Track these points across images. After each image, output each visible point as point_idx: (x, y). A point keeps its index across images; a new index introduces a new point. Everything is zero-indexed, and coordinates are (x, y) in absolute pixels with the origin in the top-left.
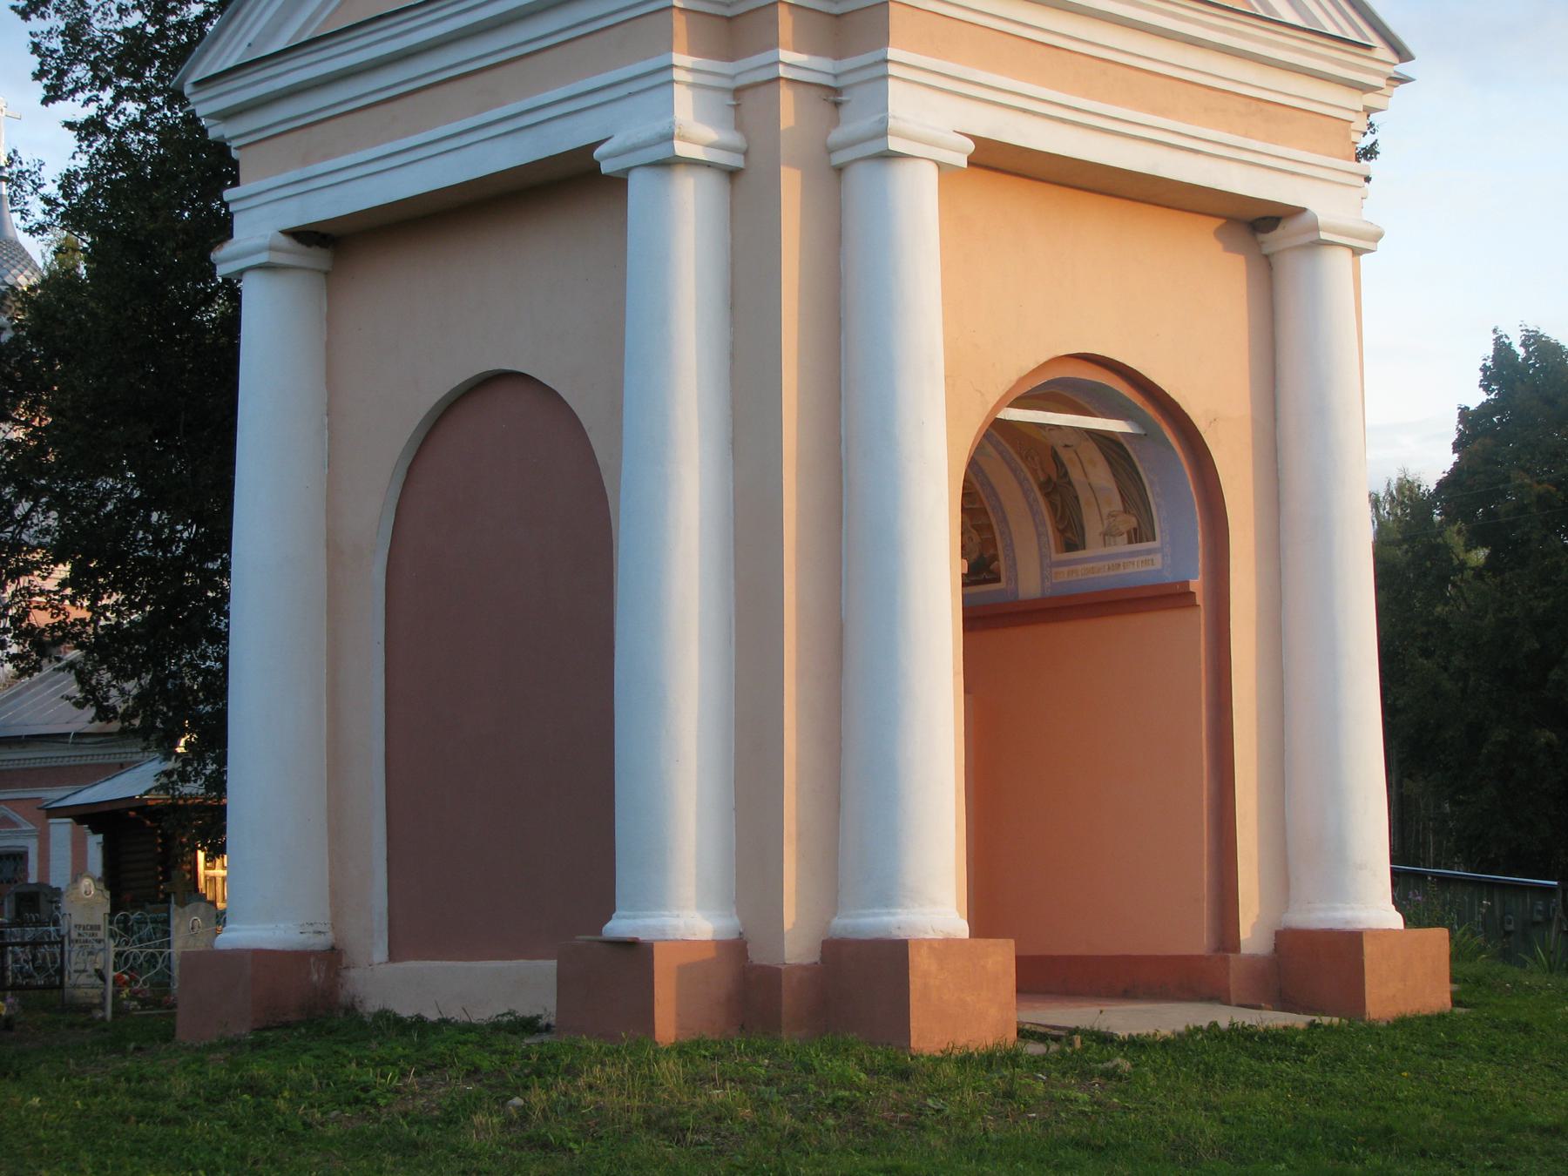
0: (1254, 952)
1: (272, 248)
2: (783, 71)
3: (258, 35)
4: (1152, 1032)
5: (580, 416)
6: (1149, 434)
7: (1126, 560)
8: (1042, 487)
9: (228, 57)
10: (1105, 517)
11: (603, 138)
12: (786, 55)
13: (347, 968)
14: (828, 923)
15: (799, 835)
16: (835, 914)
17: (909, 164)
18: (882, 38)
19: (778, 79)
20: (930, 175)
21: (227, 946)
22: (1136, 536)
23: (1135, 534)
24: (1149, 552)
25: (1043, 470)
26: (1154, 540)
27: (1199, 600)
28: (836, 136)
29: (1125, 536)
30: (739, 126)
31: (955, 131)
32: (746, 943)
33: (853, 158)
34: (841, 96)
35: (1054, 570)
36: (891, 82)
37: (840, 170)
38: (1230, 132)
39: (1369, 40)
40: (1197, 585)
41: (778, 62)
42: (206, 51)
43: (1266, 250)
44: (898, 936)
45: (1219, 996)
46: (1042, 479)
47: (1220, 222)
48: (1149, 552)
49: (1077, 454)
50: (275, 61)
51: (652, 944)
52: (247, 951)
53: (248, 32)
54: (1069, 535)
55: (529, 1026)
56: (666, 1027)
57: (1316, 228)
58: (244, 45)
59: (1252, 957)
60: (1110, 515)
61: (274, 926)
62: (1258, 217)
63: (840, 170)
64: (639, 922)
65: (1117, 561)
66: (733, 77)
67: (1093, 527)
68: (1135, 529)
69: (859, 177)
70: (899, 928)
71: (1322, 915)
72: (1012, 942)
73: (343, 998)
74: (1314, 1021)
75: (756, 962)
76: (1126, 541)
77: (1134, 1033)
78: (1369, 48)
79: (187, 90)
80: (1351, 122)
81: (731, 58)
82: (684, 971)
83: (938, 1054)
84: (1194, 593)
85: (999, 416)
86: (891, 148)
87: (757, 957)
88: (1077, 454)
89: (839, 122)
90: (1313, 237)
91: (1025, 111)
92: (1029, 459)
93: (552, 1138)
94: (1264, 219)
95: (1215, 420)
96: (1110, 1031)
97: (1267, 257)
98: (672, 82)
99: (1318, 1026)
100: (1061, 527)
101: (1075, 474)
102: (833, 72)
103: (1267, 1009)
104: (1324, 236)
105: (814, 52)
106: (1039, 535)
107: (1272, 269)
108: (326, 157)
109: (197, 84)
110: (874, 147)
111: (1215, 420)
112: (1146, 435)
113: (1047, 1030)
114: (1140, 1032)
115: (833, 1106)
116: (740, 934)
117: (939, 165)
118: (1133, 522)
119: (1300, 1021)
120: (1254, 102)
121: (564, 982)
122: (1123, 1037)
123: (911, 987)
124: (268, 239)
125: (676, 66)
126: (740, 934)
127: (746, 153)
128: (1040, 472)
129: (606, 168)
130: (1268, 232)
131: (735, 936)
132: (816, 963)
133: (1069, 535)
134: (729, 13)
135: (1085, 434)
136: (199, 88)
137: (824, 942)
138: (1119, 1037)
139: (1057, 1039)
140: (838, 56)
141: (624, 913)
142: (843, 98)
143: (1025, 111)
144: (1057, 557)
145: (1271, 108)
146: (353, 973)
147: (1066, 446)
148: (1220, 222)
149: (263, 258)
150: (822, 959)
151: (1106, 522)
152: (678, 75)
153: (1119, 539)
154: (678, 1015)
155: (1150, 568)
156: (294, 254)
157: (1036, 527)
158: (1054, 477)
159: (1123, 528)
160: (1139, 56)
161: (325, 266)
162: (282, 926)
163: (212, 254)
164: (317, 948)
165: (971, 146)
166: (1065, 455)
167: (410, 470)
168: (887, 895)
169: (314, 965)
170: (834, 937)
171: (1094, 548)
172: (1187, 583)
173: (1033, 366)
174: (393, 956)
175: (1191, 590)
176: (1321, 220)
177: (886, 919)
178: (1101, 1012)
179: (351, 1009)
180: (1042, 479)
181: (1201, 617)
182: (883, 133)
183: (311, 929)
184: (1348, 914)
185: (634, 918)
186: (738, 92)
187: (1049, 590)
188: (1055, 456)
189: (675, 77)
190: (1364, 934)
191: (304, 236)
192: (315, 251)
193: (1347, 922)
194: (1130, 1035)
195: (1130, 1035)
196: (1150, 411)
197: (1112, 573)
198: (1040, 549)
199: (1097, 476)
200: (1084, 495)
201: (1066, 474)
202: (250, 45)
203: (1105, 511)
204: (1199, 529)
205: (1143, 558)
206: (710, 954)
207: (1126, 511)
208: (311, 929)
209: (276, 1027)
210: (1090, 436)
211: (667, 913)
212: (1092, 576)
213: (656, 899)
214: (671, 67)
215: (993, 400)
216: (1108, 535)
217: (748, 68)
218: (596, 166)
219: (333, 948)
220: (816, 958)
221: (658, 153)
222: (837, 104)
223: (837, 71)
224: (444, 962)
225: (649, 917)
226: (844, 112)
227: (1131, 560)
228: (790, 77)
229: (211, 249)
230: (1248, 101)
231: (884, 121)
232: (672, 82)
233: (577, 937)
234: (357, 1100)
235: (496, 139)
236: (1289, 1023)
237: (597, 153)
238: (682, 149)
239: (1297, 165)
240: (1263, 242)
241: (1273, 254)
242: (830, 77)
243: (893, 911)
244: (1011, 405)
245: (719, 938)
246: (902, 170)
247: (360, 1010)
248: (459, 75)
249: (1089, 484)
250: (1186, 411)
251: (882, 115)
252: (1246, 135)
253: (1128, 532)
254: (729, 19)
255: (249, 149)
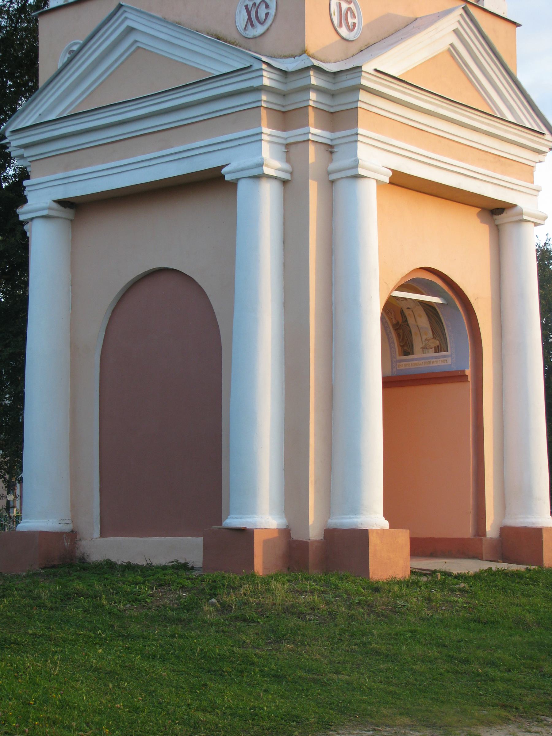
0: (491, 537)
1: (50, 208)
2: (311, 137)
3: (44, 111)
4: (466, 572)
5: (204, 289)
6: (449, 304)
7: (433, 360)
8: (394, 326)
9: (28, 120)
10: (424, 339)
11: (227, 164)
12: (313, 130)
13: (80, 540)
14: (327, 521)
15: (316, 482)
16: (329, 518)
17: (366, 180)
18: (354, 123)
19: (309, 140)
20: (374, 184)
21: (21, 530)
22: (438, 349)
23: (438, 348)
24: (445, 356)
25: (395, 318)
26: (448, 351)
27: (469, 379)
28: (332, 166)
29: (433, 349)
30: (288, 161)
31: (383, 166)
32: (290, 530)
33: (340, 177)
34: (334, 149)
35: (398, 364)
36: (359, 143)
37: (333, 182)
38: (488, 170)
39: (543, 131)
40: (468, 372)
41: (309, 133)
42: (18, 117)
43: (497, 223)
44: (361, 528)
45: (478, 557)
46: (394, 323)
47: (479, 210)
48: (445, 356)
49: (413, 312)
50: (55, 123)
51: (253, 530)
52: (37, 531)
53: (40, 108)
54: (406, 348)
55: (185, 567)
56: (259, 566)
57: (521, 214)
58: (38, 114)
59: (492, 538)
60: (426, 340)
61: (47, 521)
62: (494, 208)
63: (333, 182)
64: (244, 520)
65: (429, 360)
66: (286, 139)
67: (418, 344)
68: (438, 346)
69: (342, 186)
70: (362, 524)
71: (522, 520)
72: (408, 531)
73: (78, 553)
74: (528, 567)
75: (295, 539)
76: (434, 351)
77: (459, 572)
78: (543, 134)
79: (7, 134)
80: (534, 167)
81: (284, 130)
82: (266, 542)
83: (385, 581)
84: (467, 375)
85: (391, 295)
86: (359, 173)
87: (295, 536)
88: (413, 312)
89: (332, 160)
90: (519, 218)
91: (410, 158)
92: (389, 313)
93: (248, 617)
94: (498, 209)
95: (477, 298)
96: (450, 571)
97: (497, 226)
98: (261, 140)
99: (530, 570)
100: (401, 344)
101: (411, 321)
102: (331, 138)
103: (500, 562)
104: (525, 217)
105: (322, 129)
106: (391, 348)
107: (499, 231)
108: (77, 168)
109: (13, 132)
110: (352, 173)
111: (477, 298)
112: (447, 304)
113: (419, 570)
114: (461, 572)
115: (359, 603)
116: (287, 526)
117: (377, 181)
118: (437, 343)
119: (522, 568)
120: (497, 157)
121: (206, 547)
122: (455, 574)
123: (370, 550)
124: (48, 204)
125: (263, 133)
126: (287, 526)
127: (291, 173)
128: (394, 320)
129: (227, 178)
130: (499, 215)
131: (285, 527)
132: (322, 539)
133: (406, 348)
134: (332, 110)
135: (418, 303)
136: (14, 134)
137: (325, 530)
138: (453, 574)
139: (430, 575)
140: (333, 130)
141: (26, 520)
142: (335, 150)
143: (410, 158)
144: (399, 358)
145: (503, 159)
146: (83, 543)
147: (408, 308)
148: (479, 210)
149: (45, 213)
150: (324, 538)
151: (424, 343)
152: (264, 137)
153: (430, 350)
154: (264, 562)
155: (446, 364)
156: (59, 211)
157: (390, 344)
158: (400, 322)
159: (433, 345)
160: (454, 135)
161: (71, 217)
162: (51, 520)
163: (17, 210)
164: (66, 531)
165: (390, 173)
166: (407, 312)
167: (114, 311)
168: (355, 510)
169: (65, 538)
170: (330, 528)
171: (418, 354)
172: (464, 371)
173: (407, 272)
174: (103, 534)
175: (466, 374)
176: (524, 210)
177: (356, 520)
178: (445, 563)
179: (82, 560)
180: (394, 322)
181: (470, 386)
182: (356, 166)
183: (63, 522)
184: (534, 520)
185: (241, 518)
186: (287, 146)
187: (395, 373)
188: (402, 313)
189: (263, 138)
190: (543, 529)
191: (64, 203)
192: (68, 210)
193: (534, 524)
194: (458, 573)
195: (458, 573)
196: (450, 293)
197: (426, 366)
198: (391, 353)
199: (423, 322)
200: (414, 330)
201: (406, 321)
202: (40, 115)
203: (424, 337)
204: (469, 347)
205: (441, 359)
206: (276, 535)
207: (434, 338)
208: (63, 522)
209: (49, 567)
210: (420, 304)
211: (256, 516)
212: (416, 367)
213: (252, 510)
214: (261, 133)
215: (392, 286)
216: (425, 349)
217: (294, 135)
218: (223, 176)
219: (72, 531)
220: (321, 537)
221: (255, 172)
222: (331, 153)
223: (333, 138)
224: (129, 538)
225: (248, 518)
226: (334, 156)
227: (436, 360)
228: (313, 140)
229: (17, 207)
230: (495, 156)
231: (357, 161)
232: (261, 140)
233: (213, 527)
234: (136, 600)
235: (171, 162)
236: (519, 569)
237: (223, 171)
238: (267, 171)
239: (514, 185)
240: (496, 219)
241: (500, 225)
242: (329, 140)
243: (358, 516)
244: (397, 290)
245: (279, 528)
246: (361, 182)
247: (88, 560)
248: (150, 133)
249: (417, 325)
250: (466, 294)
251: (355, 158)
252: (494, 171)
253: (435, 348)
254: (284, 113)
255: (35, 163)
